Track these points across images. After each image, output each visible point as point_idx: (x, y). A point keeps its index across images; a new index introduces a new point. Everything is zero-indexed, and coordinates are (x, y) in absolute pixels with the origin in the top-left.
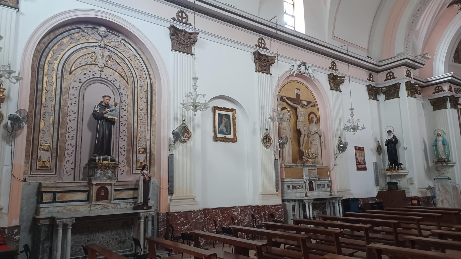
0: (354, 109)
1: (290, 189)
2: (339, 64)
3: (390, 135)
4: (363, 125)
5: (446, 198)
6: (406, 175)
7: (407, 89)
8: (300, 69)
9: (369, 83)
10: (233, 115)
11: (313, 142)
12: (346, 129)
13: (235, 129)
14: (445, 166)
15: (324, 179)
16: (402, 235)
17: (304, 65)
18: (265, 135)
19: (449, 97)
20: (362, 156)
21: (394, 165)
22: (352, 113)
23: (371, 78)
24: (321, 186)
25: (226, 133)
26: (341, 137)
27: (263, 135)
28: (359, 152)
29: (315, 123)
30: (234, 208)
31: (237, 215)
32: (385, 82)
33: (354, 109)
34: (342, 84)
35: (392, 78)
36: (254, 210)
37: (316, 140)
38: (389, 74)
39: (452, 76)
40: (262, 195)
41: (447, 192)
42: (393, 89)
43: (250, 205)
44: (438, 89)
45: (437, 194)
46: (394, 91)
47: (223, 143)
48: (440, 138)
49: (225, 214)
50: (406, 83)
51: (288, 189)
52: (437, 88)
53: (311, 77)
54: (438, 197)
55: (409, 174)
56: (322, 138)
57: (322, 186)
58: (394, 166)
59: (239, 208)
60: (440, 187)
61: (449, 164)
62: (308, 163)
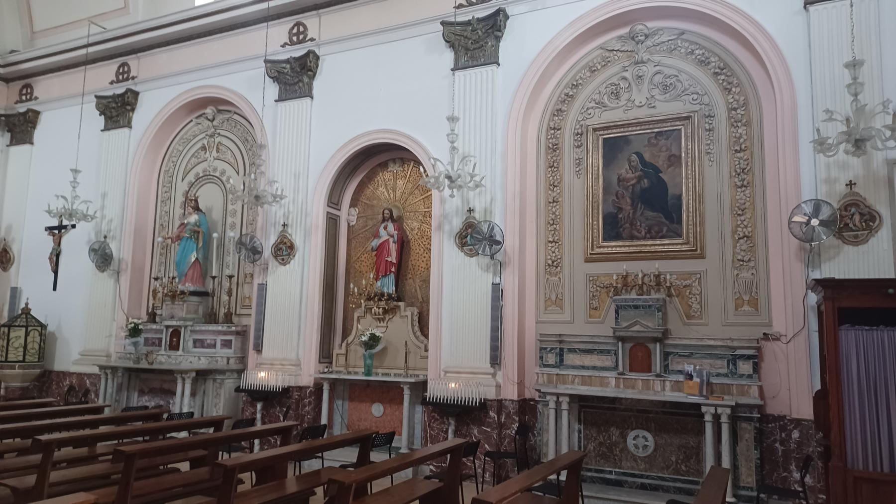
4: (49, 206)
16: (159, 460)
38: (296, 28)
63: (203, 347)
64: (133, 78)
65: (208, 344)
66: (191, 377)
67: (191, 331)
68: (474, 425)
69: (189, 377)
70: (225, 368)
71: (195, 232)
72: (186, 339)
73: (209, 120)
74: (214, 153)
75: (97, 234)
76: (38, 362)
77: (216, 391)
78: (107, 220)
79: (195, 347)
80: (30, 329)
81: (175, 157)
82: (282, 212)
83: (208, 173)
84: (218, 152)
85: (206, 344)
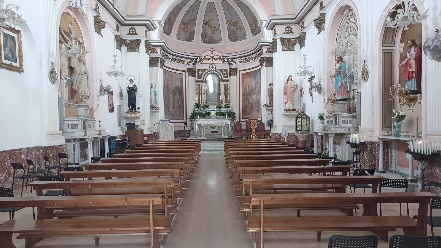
0: (117, 56)
1: (69, 129)
2: (101, 8)
6: (140, 117)
7: (146, 47)
9: (117, 33)
10: (19, 39)
12: (109, 74)
13: (21, 56)
14: (154, 111)
18: (51, 69)
19: (160, 58)
20: (111, 100)
21: (134, 108)
23: (117, 29)
25: (12, 59)
27: (49, 69)
30: (20, 150)
31: (24, 158)
32: (128, 35)
33: (117, 56)
34: (103, 29)
35: (134, 34)
36: (41, 151)
39: (164, 43)
40: (50, 134)
43: (35, 146)
44: (154, 51)
46: (136, 46)
47: (8, 72)
49: (13, 157)
50: (145, 41)
51: (68, 129)
53: (84, 14)
54: (161, 134)
56: (88, 78)
58: (134, 110)
59: (25, 150)
60: (163, 127)
61: (158, 110)
62: (83, 103)
66: (333, 136)
68: (437, 167)
69: (331, 136)
71: (339, 72)
72: (340, 120)
74: (350, 32)
76: (307, 131)
79: (343, 124)
80: (302, 118)
81: (339, 38)
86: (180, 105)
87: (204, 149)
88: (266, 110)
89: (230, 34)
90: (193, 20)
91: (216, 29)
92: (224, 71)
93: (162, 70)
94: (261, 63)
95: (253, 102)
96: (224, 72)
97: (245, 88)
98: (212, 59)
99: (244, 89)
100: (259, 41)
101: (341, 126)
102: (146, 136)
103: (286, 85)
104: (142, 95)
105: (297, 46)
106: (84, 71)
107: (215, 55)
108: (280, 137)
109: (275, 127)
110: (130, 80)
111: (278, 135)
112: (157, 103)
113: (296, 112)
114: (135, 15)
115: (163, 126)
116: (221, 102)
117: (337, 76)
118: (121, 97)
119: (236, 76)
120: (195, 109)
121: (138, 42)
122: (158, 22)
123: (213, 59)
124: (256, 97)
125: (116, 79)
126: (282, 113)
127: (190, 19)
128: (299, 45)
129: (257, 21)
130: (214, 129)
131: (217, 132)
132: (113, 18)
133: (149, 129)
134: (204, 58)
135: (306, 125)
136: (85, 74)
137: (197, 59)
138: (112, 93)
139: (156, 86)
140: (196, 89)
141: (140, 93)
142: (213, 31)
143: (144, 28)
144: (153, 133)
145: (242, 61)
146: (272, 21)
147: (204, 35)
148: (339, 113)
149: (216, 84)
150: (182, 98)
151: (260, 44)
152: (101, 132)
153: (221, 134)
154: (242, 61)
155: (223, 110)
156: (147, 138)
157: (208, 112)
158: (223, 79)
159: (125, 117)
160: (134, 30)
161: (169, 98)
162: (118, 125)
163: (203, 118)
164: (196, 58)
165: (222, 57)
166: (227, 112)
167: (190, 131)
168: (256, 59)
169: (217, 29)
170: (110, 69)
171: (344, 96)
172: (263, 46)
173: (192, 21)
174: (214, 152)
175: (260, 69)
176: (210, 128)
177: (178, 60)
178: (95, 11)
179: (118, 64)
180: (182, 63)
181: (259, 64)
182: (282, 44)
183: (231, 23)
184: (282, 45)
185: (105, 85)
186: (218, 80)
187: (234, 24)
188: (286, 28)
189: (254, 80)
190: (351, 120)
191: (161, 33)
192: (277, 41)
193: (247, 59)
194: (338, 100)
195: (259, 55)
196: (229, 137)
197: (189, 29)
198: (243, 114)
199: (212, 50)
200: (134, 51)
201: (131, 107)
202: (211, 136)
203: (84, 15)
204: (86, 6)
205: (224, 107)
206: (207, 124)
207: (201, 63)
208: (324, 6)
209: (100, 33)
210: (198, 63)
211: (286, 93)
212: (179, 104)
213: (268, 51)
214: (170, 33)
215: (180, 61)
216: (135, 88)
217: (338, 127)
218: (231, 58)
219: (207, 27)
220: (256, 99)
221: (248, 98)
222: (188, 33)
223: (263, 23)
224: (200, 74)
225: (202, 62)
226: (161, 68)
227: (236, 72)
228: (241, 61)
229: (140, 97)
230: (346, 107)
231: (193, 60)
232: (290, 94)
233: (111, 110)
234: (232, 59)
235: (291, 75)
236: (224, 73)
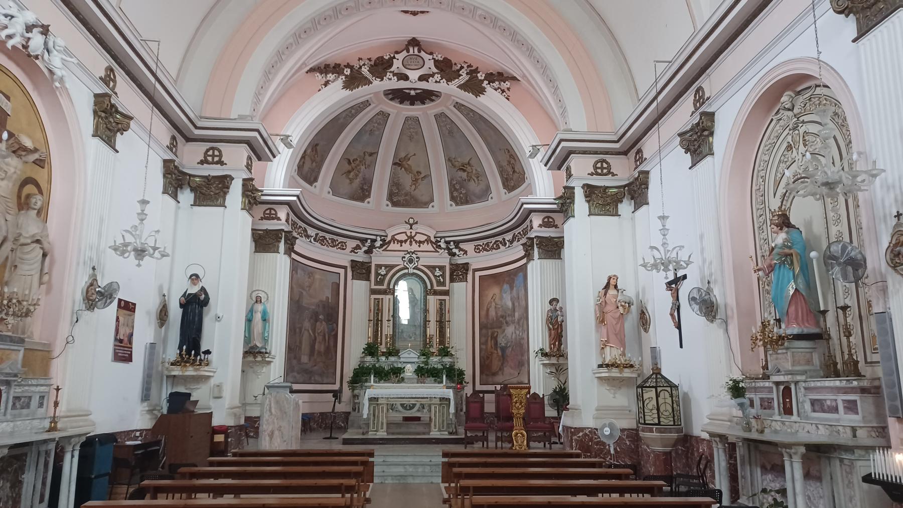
2: (121, 78)
3: (195, 284)
5: (281, 427)
7: (244, 195)
8: (29, 39)
9: (169, 156)
11: (19, 265)
12: (121, 249)
14: (259, 362)
15: (34, 382)
17: (42, 33)
19: (286, 232)
20: (127, 326)
21: (193, 352)
22: (143, 211)
23: (173, 146)
24: (20, 401)
26: (96, 268)
28: (125, 314)
29: (36, 211)
33: (668, 217)
35: (217, 163)
37: (32, 262)
39: (298, 196)
41: (283, 412)
42: (215, 185)
44: (270, 214)
45: (264, 419)
46: (217, 192)
48: (259, 308)
50: (244, 180)
52: (268, 212)
54: (264, 426)
55: (215, 375)
56: (48, 259)
57: (23, 402)
58: (192, 356)
60: (272, 405)
61: (267, 359)
63: (824, 411)
64: (708, 98)
65: (829, 407)
66: (799, 453)
67: (806, 389)
69: (795, 453)
70: (851, 443)
71: (786, 255)
72: (801, 399)
73: (789, 110)
75: (702, 280)
76: (674, 425)
77: (847, 477)
78: (707, 263)
79: (814, 411)
80: (659, 389)
81: (763, 170)
82: (892, 196)
83: (799, 176)
84: (805, 145)
85: (826, 407)
86: (328, 349)
87: (383, 472)
88: (543, 364)
89: (453, 189)
90: (371, 154)
91: (421, 177)
92: (437, 269)
93: (288, 260)
94: (526, 251)
95: (506, 344)
96: (438, 273)
97: (488, 310)
98: (411, 242)
99: (483, 313)
100: (523, 201)
101: (807, 418)
102: (223, 430)
103: (603, 300)
104: (221, 315)
105: (625, 207)
106: (33, 236)
107: (417, 233)
108: (591, 440)
109: (576, 409)
110: (191, 276)
111: (586, 435)
112: (268, 340)
113: (632, 372)
114: (222, 116)
115: (272, 402)
116: (430, 342)
117: (780, 266)
118: (160, 319)
119: (465, 283)
120: (363, 357)
121: (224, 182)
122: (282, 137)
123: (414, 242)
124: (515, 333)
125: (137, 265)
126: (594, 373)
127: (364, 153)
128: (630, 204)
129: (516, 158)
130: (410, 409)
131: (418, 419)
132: (152, 105)
133: (233, 410)
134: (392, 239)
135: (671, 410)
136: (34, 245)
137: (375, 240)
138: (131, 306)
139: (268, 299)
140: (370, 310)
141: (218, 312)
142: (415, 181)
143: (243, 152)
144: (242, 422)
145: (481, 248)
146: (563, 144)
147: (394, 188)
148: (799, 378)
149: (417, 300)
150: (333, 330)
151: (525, 206)
152: (56, 423)
153: (428, 425)
154: (481, 248)
155: (435, 361)
156: (223, 435)
157: (396, 365)
158: (436, 288)
159: (167, 377)
160: (216, 153)
161: (300, 329)
162: (142, 400)
163: (382, 381)
164: (374, 237)
165: (435, 237)
166: (445, 368)
167: (349, 413)
168: (515, 243)
169: (425, 177)
170: (123, 236)
171: (807, 327)
172: (532, 211)
173: (367, 157)
174: (410, 480)
175: (525, 265)
176: (400, 408)
177: (330, 241)
178: (169, 151)
179: (151, 224)
180: (339, 248)
181: (523, 253)
182: (588, 199)
183: (456, 163)
184: (588, 202)
185: (103, 282)
186: (424, 291)
187: (464, 166)
188: (597, 162)
189: (509, 292)
190: (856, 401)
191: (293, 177)
192: (574, 193)
193: (491, 244)
194: (791, 339)
195: (521, 235)
196: (450, 433)
197: (360, 175)
198: (481, 372)
199: (411, 221)
200: (211, 203)
201: (184, 347)
202: (403, 430)
203: (56, 81)
204: (64, 57)
205: (436, 356)
206: (393, 398)
207: (385, 250)
208: (707, 96)
209: (110, 142)
210: (377, 249)
211: (603, 319)
212: (327, 344)
213: (547, 224)
214: (316, 180)
215: (333, 243)
216: (203, 296)
217: (798, 419)
218: (454, 242)
219: (401, 172)
220: (513, 337)
221: (495, 335)
222: (357, 182)
223: (539, 149)
224: (382, 275)
225: (387, 248)
226: (286, 256)
227: (467, 274)
228: (478, 249)
229: (217, 323)
230: (816, 359)
231: (367, 242)
232: (614, 323)
233: (120, 354)
234: (457, 243)
235: (615, 276)
236: (438, 274)
